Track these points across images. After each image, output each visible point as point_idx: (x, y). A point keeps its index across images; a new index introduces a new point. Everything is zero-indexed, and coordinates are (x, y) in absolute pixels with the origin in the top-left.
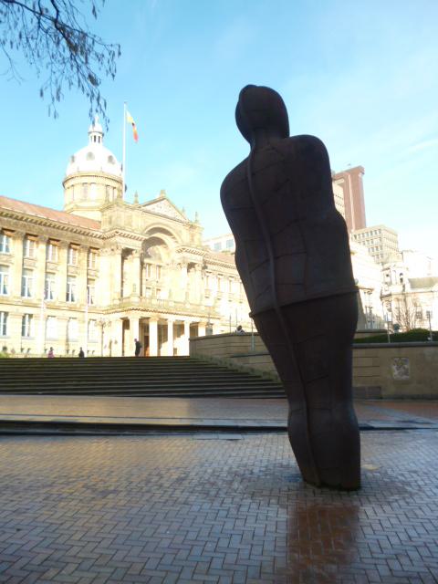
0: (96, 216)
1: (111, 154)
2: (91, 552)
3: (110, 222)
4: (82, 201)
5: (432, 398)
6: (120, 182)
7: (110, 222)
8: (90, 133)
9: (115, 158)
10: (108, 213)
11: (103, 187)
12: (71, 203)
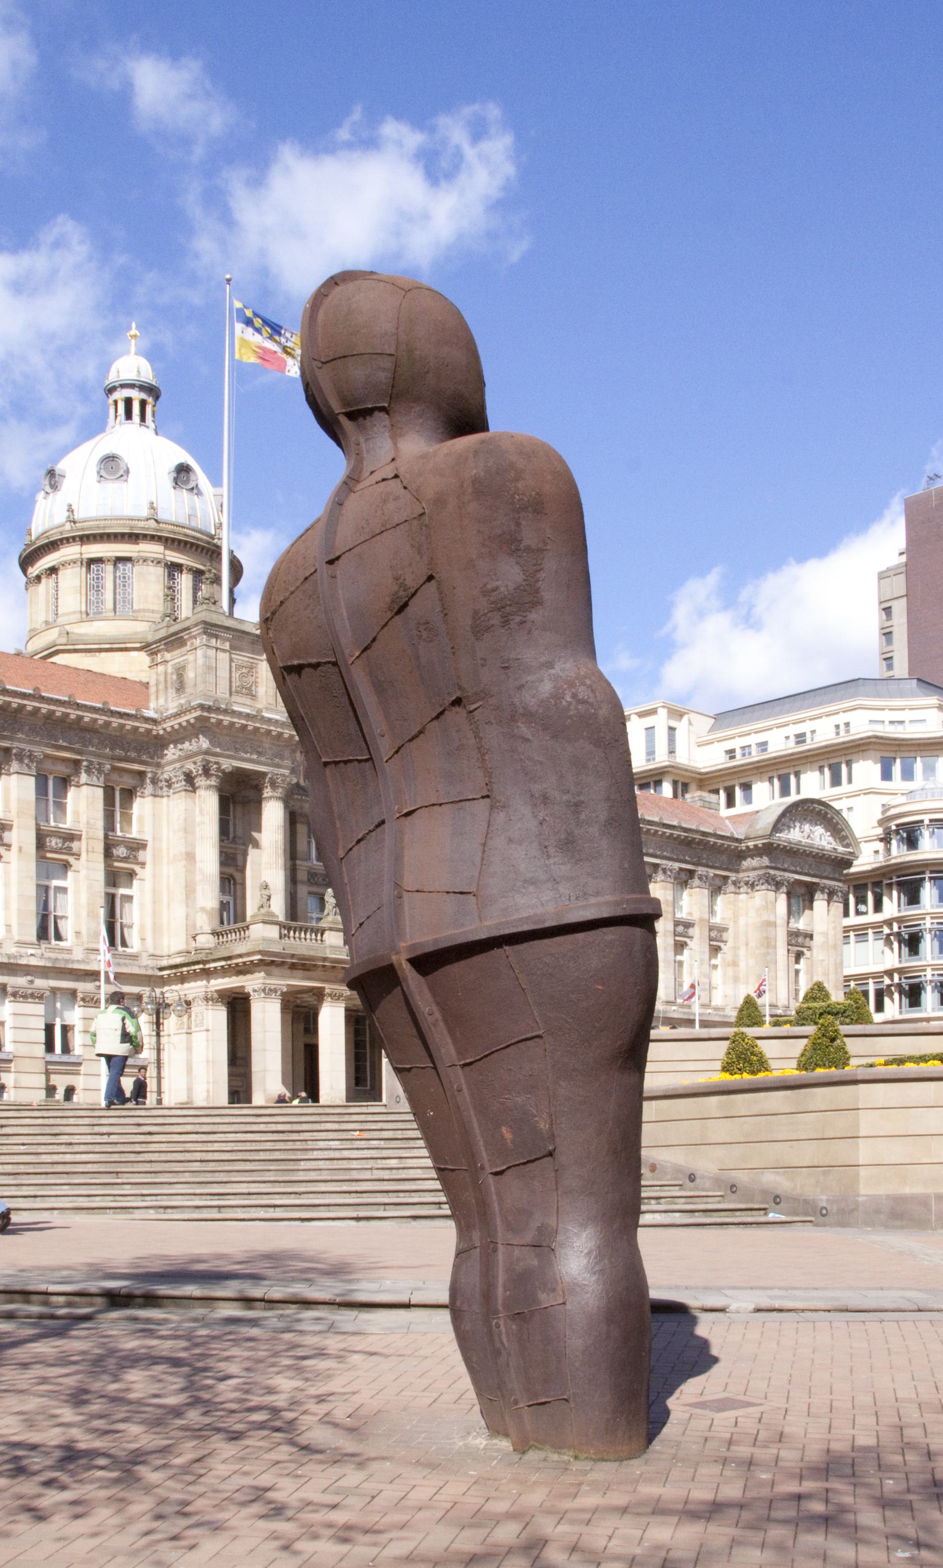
0: (133, 666)
1: (185, 457)
2: (701, 1394)
3: (180, 687)
4: (87, 616)
5: (10, 1293)
6: (211, 551)
7: (180, 687)
8: (111, 390)
9: (201, 477)
10: (173, 657)
11: (160, 571)
12: (48, 625)
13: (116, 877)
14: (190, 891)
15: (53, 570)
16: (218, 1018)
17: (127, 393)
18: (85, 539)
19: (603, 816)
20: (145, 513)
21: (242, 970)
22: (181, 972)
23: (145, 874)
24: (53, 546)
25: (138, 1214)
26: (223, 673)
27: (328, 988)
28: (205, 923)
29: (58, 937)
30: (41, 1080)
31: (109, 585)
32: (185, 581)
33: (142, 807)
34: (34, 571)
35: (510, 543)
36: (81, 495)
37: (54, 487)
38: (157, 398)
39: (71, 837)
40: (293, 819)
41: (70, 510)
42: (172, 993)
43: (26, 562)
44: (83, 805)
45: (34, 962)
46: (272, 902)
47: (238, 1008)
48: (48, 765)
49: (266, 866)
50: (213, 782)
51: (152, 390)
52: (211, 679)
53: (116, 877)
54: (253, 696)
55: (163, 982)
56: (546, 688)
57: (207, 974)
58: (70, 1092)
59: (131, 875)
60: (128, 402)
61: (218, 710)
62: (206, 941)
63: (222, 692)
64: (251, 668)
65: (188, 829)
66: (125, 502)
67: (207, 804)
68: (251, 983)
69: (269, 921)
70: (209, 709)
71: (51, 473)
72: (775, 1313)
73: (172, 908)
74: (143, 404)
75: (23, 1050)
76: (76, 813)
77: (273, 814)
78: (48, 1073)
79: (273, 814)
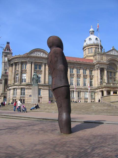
0: (92, 58)
4: (89, 54)
7: (96, 60)
8: (90, 32)
10: (95, 57)
13: (91, 79)
14: (98, 80)
15: (85, 49)
16: (101, 93)
17: (91, 32)
18: (88, 46)
19: (63, 78)
20: (93, 43)
21: (103, 88)
22: (97, 89)
23: (94, 79)
24: (85, 47)
25: (73, 113)
26: (100, 58)
27: (111, 90)
28: (99, 83)
29: (86, 85)
30: (84, 100)
31: (90, 50)
32: (97, 49)
33: (93, 72)
34: (84, 50)
35: (56, 57)
36: (88, 42)
37: (85, 42)
38: (94, 32)
39: (87, 75)
40: (108, 72)
41: (87, 44)
42: (97, 90)
43: (83, 49)
44: (88, 72)
45: (83, 88)
46: (105, 81)
47: (102, 92)
48: (84, 69)
49: (105, 78)
50: (99, 69)
51: (93, 31)
52: (99, 59)
53: (91, 79)
54: (103, 60)
55: (96, 90)
56: (59, 68)
57: (99, 89)
58: (87, 101)
59: (92, 79)
60: (91, 33)
61: (99, 62)
62: (99, 85)
63: (100, 60)
64: (103, 57)
65: (97, 74)
66: (91, 42)
67: (99, 71)
68: (103, 89)
69: (105, 83)
70: (99, 62)
71: (85, 40)
72: (81, 121)
73: (96, 82)
74: (93, 33)
75: (82, 97)
76: (87, 73)
77: (105, 72)
78: (85, 99)
79: (105, 72)
